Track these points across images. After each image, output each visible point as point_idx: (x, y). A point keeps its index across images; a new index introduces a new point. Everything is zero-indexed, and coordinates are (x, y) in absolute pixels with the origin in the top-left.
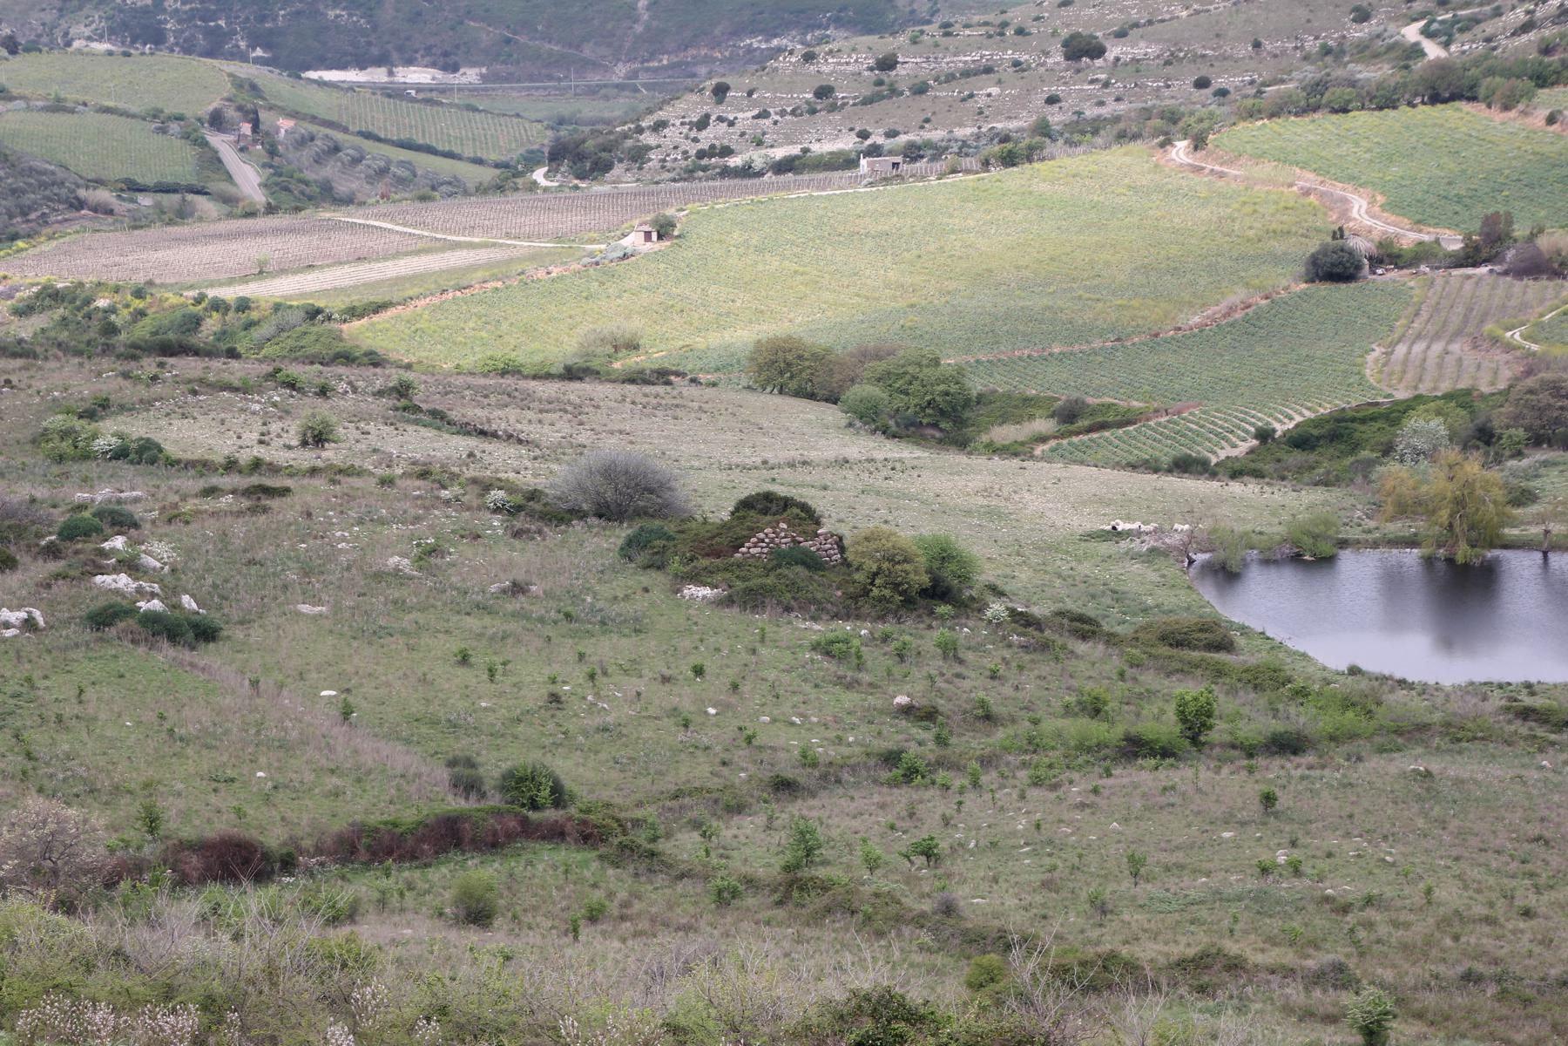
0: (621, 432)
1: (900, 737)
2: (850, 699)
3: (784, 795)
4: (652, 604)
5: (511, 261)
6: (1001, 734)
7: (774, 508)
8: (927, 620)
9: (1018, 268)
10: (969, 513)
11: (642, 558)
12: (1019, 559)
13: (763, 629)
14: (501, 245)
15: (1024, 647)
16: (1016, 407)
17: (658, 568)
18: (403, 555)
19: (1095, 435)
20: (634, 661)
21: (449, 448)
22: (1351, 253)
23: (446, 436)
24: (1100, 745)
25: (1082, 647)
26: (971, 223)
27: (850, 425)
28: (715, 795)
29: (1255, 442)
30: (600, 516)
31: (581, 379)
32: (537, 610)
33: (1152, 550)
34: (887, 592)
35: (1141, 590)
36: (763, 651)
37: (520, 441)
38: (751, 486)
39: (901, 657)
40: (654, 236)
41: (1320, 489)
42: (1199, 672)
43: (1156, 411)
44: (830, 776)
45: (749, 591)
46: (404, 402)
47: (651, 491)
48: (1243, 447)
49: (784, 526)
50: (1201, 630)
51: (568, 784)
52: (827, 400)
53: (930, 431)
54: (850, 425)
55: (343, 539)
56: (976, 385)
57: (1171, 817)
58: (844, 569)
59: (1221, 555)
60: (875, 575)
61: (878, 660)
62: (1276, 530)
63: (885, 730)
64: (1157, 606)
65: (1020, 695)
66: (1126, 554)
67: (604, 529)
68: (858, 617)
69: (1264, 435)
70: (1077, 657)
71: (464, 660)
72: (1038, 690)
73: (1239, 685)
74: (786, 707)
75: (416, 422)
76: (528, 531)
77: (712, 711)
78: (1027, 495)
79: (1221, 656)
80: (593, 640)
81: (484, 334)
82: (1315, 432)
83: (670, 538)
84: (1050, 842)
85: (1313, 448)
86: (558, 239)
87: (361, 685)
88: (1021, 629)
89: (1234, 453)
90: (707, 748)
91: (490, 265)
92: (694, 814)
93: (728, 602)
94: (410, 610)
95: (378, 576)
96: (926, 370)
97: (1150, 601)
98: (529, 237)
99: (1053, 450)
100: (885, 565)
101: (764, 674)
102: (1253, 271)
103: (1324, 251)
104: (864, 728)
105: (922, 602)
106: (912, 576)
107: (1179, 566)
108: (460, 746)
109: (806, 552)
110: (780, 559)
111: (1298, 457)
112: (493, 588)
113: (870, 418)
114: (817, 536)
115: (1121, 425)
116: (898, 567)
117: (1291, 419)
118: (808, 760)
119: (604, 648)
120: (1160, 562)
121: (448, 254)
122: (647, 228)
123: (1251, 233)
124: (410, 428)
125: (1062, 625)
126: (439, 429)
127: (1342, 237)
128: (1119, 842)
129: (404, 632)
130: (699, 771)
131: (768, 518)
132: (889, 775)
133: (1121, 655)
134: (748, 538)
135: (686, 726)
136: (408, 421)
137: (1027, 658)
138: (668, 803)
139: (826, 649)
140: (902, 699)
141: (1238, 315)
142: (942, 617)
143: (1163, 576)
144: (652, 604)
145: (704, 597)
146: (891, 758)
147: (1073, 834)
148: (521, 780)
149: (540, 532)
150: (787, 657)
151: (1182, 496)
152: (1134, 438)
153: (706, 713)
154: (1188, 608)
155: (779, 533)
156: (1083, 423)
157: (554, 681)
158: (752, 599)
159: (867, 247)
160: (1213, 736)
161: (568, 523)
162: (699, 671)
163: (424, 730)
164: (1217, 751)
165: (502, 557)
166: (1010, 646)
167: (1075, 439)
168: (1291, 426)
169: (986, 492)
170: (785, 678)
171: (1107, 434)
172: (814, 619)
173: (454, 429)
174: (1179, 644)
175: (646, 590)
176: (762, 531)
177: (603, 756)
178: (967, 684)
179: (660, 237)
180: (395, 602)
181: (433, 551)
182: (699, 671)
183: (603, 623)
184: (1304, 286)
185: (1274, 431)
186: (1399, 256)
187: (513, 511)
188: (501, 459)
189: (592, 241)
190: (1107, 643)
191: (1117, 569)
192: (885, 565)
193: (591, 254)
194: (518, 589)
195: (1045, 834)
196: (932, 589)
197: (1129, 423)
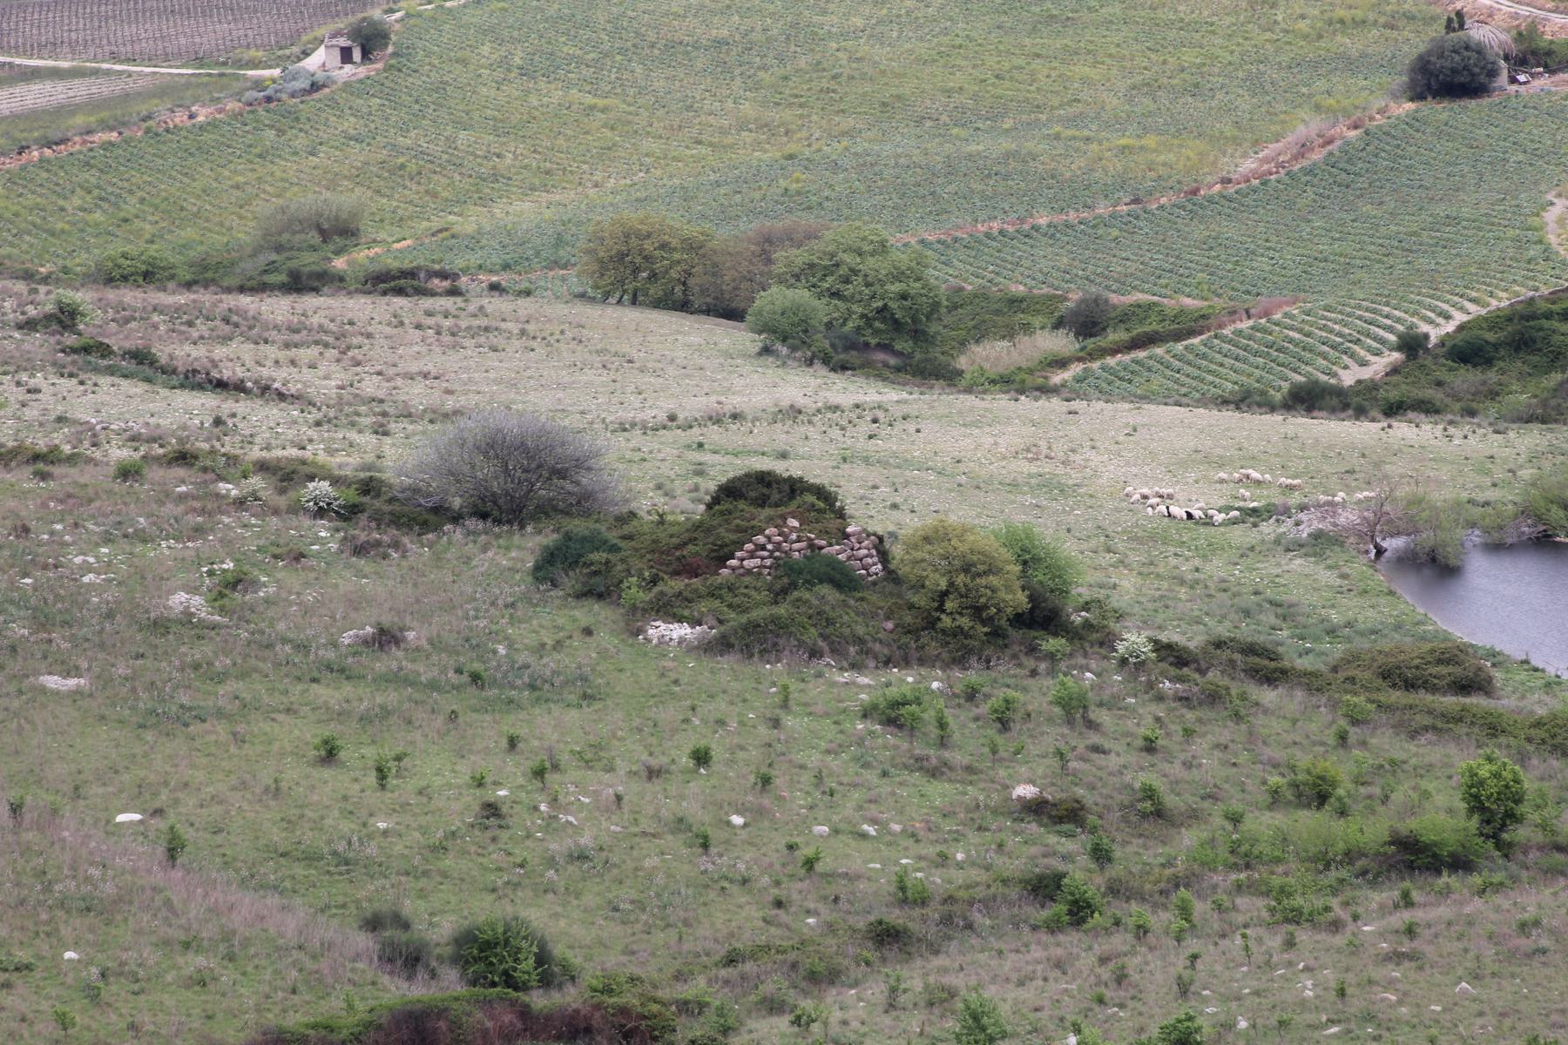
0: (426, 376)
1: (1034, 850)
2: (940, 792)
3: (892, 952)
4: (603, 654)
5: (126, 97)
6: (1189, 838)
7: (775, 496)
8: (1030, 663)
9: (948, 92)
10: (1014, 485)
11: (571, 581)
12: (1110, 558)
13: (785, 688)
14: (108, 73)
15: (1184, 700)
16: (997, 312)
17: (600, 597)
18: (193, 590)
19: (1141, 354)
20: (597, 747)
21: (185, 412)
22: (1479, 50)
23: (164, 392)
24: (1350, 856)
25: (1269, 696)
26: (858, 22)
27: (766, 351)
28: (792, 956)
29: (1397, 356)
30: (484, 516)
31: (316, 290)
32: (426, 673)
33: (1317, 536)
34: (965, 622)
35: (1314, 599)
36: (789, 721)
37: (282, 396)
38: (724, 469)
39: (1004, 724)
40: (357, 55)
41: (1536, 427)
42: (1462, 729)
43: (1233, 313)
44: (955, 918)
45: (753, 628)
46: (70, 340)
47: (562, 474)
48: (1378, 366)
49: (794, 523)
50: (1440, 662)
51: (558, 950)
52: (708, 312)
53: (880, 356)
54: (766, 351)
55: (86, 568)
56: (942, 277)
57: (1550, 971)
58: (890, 587)
59: (1427, 538)
60: (944, 595)
61: (970, 737)
62: (1507, 497)
63: (1013, 842)
64: (1349, 625)
65: (1195, 774)
66: (1277, 542)
67: (498, 536)
68: (922, 662)
69: (1412, 345)
70: (1266, 712)
71: (330, 754)
72: (1223, 764)
73: (1531, 748)
74: (848, 809)
75: (110, 371)
76: (378, 544)
77: (737, 820)
78: (1092, 454)
79: (1476, 701)
80: (522, 715)
81: (98, 216)
82: (1491, 337)
83: (614, 549)
84: (1369, 1018)
85: (1489, 362)
86: (199, 61)
87: (176, 802)
88: (1173, 671)
89: (1366, 374)
90: (745, 881)
91: (93, 105)
92: (768, 988)
93: (721, 645)
94: (221, 678)
95: (160, 626)
96: (871, 261)
97: (1335, 617)
98: (151, 60)
99: (1079, 380)
100: (960, 579)
101: (799, 757)
102: (1321, 85)
103: (1439, 50)
104: (974, 837)
105: (1015, 634)
106: (1002, 594)
107: (1363, 559)
108: (372, 893)
109: (833, 563)
110: (790, 577)
111: (1465, 378)
112: (347, 638)
113: (789, 339)
114: (847, 536)
115: (1178, 336)
116: (983, 581)
117: (1448, 317)
118: (907, 896)
119: (553, 727)
120: (1336, 555)
121: (18, 90)
122: (343, 42)
123: (1302, 25)
124: (104, 381)
125: (1232, 663)
126: (148, 380)
127: (1462, 26)
128: (1481, 1014)
129: (220, 714)
130: (743, 919)
131: (768, 512)
132: (1045, 914)
133: (1334, 705)
134: (739, 545)
135: (705, 846)
136: (97, 370)
137: (1190, 716)
138: (723, 973)
139: (893, 715)
140: (1025, 791)
141: (1317, 156)
142: (1051, 657)
143: (1344, 576)
144: (603, 654)
145: (681, 640)
146: (1044, 887)
147: (1400, 1002)
148: (488, 945)
149: (396, 545)
150: (828, 729)
151: (1331, 447)
152: (1204, 357)
153: (728, 823)
154: (1398, 627)
155: (787, 535)
156: (1115, 336)
157: (480, 783)
158: (749, 640)
159: (699, 65)
160: (1520, 834)
161: (437, 528)
162: (701, 758)
163: (299, 870)
164: (1533, 855)
165: (336, 589)
166: (1160, 698)
167: (1111, 361)
168: (1450, 327)
169: (1030, 452)
170: (833, 763)
171: (1159, 351)
172: (854, 666)
173: (175, 381)
174: (1410, 685)
175: (588, 632)
176: (761, 532)
177: (590, 899)
178: (1113, 761)
179: (366, 54)
180: (196, 667)
181: (236, 582)
182: (701, 758)
183: (532, 687)
184: (1410, 106)
185: (1426, 336)
186: (1549, 53)
187: (349, 513)
188: (265, 429)
189: (255, 64)
190: (1309, 689)
191: (1268, 568)
192: (960, 579)
193: (258, 85)
194: (386, 638)
195: (1356, 1005)
196: (998, 614)
197: (1192, 333)
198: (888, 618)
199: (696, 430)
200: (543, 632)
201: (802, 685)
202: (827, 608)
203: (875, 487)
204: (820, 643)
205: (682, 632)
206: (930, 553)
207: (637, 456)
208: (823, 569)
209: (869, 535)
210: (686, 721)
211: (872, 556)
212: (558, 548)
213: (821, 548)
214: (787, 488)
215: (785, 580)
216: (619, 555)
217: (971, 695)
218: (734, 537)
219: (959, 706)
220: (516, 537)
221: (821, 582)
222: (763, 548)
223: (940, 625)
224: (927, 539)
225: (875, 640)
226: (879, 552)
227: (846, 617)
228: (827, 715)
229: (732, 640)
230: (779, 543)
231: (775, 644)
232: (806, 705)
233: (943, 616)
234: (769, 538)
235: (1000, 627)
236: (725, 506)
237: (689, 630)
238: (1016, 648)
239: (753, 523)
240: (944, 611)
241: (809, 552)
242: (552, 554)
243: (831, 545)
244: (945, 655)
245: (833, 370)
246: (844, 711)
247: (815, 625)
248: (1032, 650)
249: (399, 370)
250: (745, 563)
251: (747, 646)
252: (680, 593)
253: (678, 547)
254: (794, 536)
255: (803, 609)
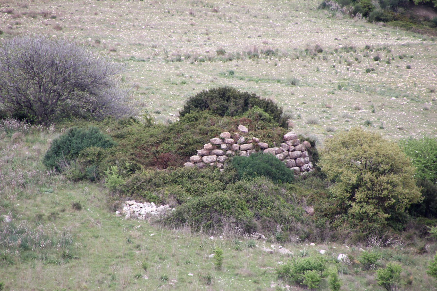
4: (85, 224)
7: (232, 108)
8: (420, 243)
11: (72, 168)
13: (219, 254)
17: (93, 180)
30: (20, 117)
34: (370, 209)
45: (202, 207)
47: (83, 87)
49: (243, 128)
53: (422, 12)
58: (317, 180)
60: (355, 187)
67: (26, 133)
68: (334, 239)
80: (12, 269)
83: (106, 144)
93: (178, 220)
100: (367, 176)
105: (412, 220)
106: (400, 189)
109: (271, 160)
110: (239, 169)
114: (284, 140)
131: (226, 119)
134: (201, 144)
145: (148, 215)
155: (236, 138)
158: (205, 217)
175: (77, 207)
176: (218, 134)
192: (367, 176)
198: (310, 204)
199: (234, 62)
200: (43, 206)
201: (234, 253)
202: (262, 195)
203: (358, 109)
204: (255, 221)
205: (149, 209)
206: (345, 154)
207: (179, 80)
208: (263, 165)
209: (302, 140)
210: (138, 277)
211: (305, 157)
212: (64, 143)
213: (263, 149)
214: (242, 101)
215: (233, 172)
216: (109, 150)
217: (369, 264)
218: (197, 137)
219: (357, 273)
220: (42, 135)
221: (260, 174)
222: (219, 147)
223: (350, 211)
224: (344, 144)
225: (298, 220)
226: (310, 153)
227: (277, 202)
228: (250, 275)
229: (186, 216)
230: (231, 144)
231: (219, 221)
232: (234, 268)
233: (353, 204)
234: (223, 140)
235: (401, 215)
236: (193, 114)
237: (155, 208)
238: (412, 231)
239: (214, 127)
240: (354, 200)
241: (254, 151)
242: (59, 147)
243: (272, 147)
244: (353, 234)
245: (370, 21)
246: (264, 273)
247: (251, 208)
248: (424, 234)
249: (28, 11)
250: (205, 158)
251: (197, 221)
252: (150, 180)
253: (159, 143)
254: (243, 139)
255: (243, 195)
